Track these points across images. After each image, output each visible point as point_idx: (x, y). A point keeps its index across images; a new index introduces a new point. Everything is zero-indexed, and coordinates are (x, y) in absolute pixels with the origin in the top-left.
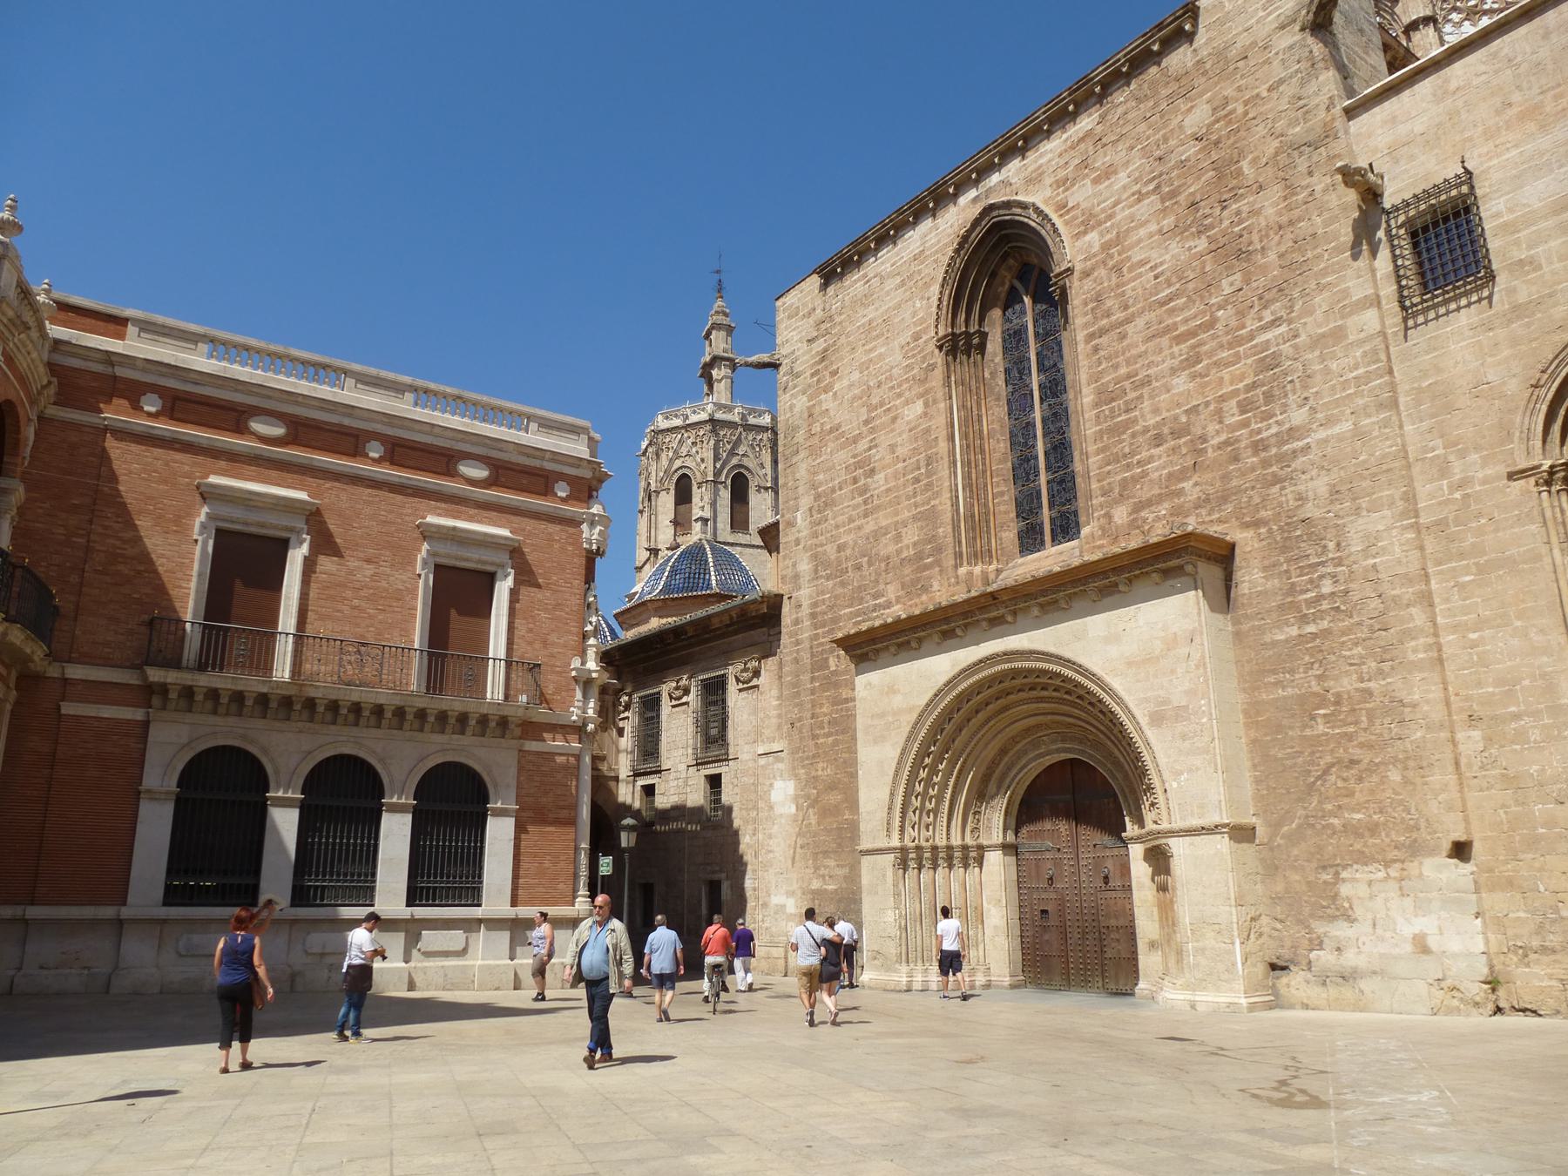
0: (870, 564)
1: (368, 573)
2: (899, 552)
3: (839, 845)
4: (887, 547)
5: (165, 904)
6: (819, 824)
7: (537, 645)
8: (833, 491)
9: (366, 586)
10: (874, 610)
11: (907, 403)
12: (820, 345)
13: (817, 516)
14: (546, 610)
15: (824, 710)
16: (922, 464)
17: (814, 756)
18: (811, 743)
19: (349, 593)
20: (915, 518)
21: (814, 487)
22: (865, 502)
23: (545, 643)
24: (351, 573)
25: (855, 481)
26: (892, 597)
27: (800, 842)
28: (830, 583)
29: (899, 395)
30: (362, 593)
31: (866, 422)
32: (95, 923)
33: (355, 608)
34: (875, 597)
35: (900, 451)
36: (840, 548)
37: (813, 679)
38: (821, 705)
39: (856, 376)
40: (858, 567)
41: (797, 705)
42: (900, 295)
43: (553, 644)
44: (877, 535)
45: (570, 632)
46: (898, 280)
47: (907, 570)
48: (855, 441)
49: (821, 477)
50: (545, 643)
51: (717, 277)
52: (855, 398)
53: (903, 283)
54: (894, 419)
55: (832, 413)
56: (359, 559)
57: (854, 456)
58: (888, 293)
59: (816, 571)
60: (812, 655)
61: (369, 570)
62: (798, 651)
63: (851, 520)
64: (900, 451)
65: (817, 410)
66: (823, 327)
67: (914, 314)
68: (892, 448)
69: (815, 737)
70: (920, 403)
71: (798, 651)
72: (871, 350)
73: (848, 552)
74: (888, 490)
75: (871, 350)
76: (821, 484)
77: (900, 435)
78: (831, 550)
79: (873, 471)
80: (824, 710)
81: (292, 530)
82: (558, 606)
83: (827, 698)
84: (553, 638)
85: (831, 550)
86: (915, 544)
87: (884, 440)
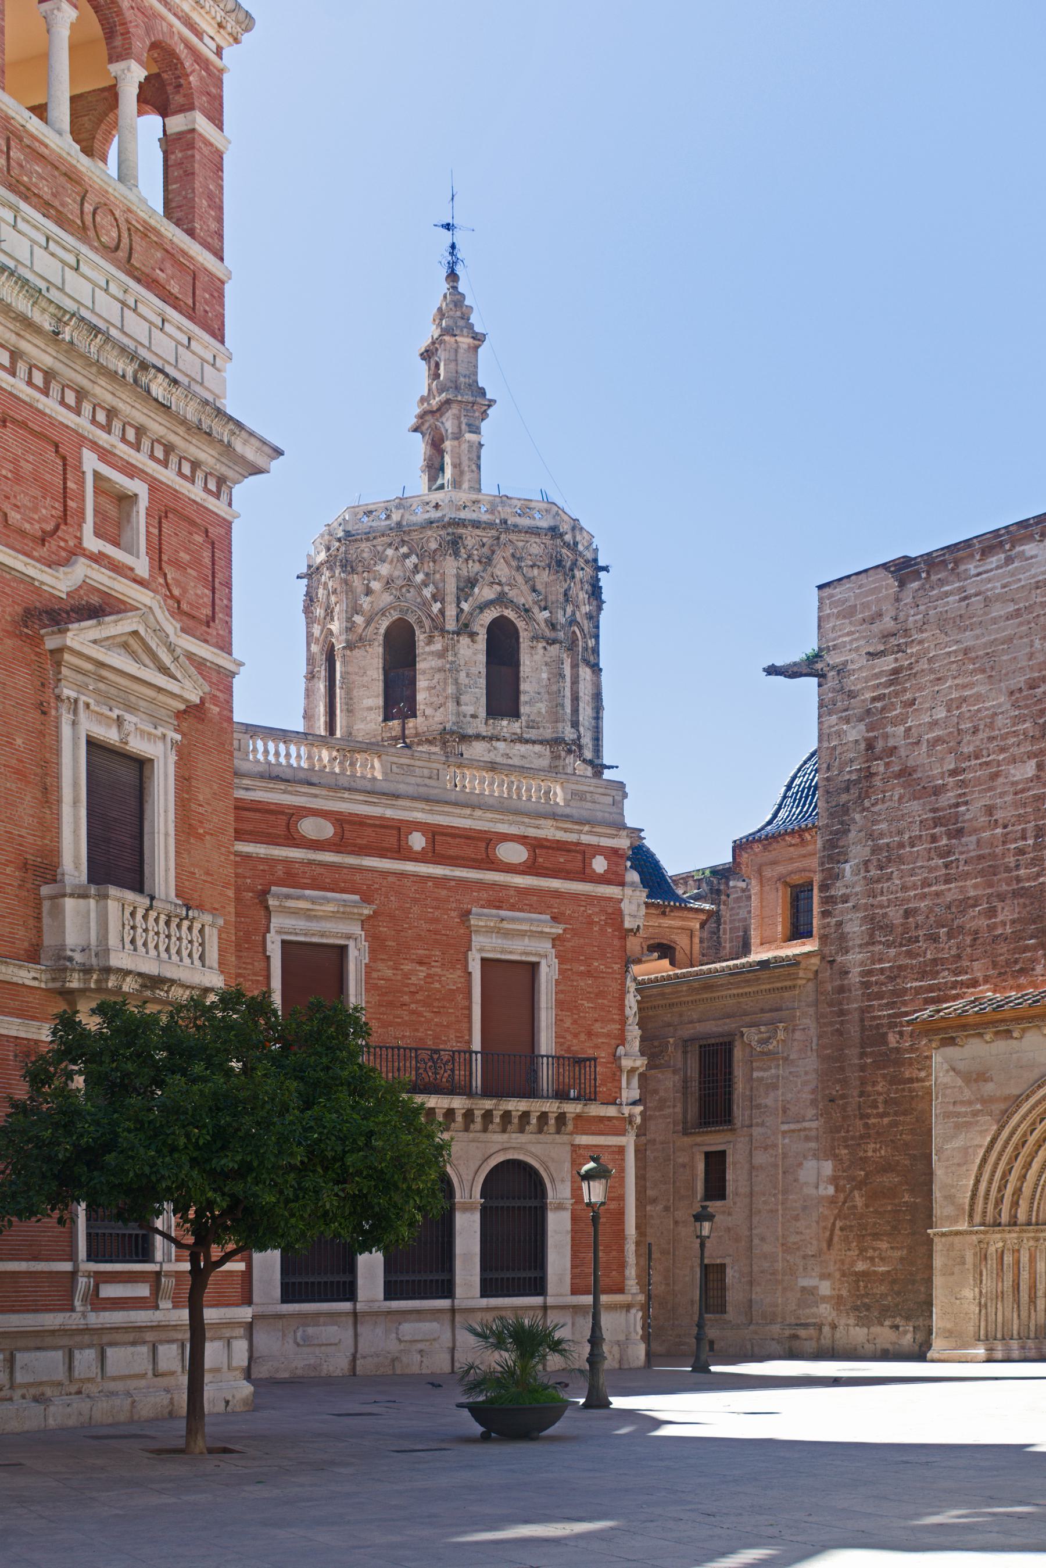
0: (950, 935)
1: (422, 975)
2: (991, 928)
3: (894, 1228)
4: (975, 920)
5: (483, 1295)
6: (867, 1206)
7: (583, 1037)
8: (901, 845)
9: (421, 988)
10: (953, 988)
11: (1014, 760)
12: (888, 663)
13: (874, 872)
14: (589, 999)
15: (879, 1088)
16: (1030, 833)
17: (862, 1137)
18: (859, 1123)
19: (406, 998)
20: (1015, 894)
21: (870, 836)
22: (947, 866)
23: (590, 1034)
24: (406, 976)
25: (934, 839)
26: (979, 975)
27: (839, 1224)
28: (892, 952)
29: (1003, 750)
30: (418, 997)
31: (954, 773)
32: (331, 1315)
33: (413, 1012)
34: (957, 972)
35: (999, 815)
36: (907, 914)
37: (863, 1055)
38: (874, 1084)
39: (941, 714)
40: (934, 938)
41: (839, 1081)
42: (1011, 628)
43: (598, 1035)
44: (966, 904)
45: (613, 1021)
46: (1012, 607)
47: (1003, 948)
48: (937, 791)
49: (883, 826)
50: (590, 1034)
51: (446, 237)
52: (938, 740)
53: (1017, 613)
54: (994, 776)
55: (903, 753)
56: (413, 961)
57: (934, 810)
58: (994, 621)
59: (872, 935)
60: (863, 1029)
61: (422, 972)
62: (842, 1023)
63: (926, 883)
64: (999, 815)
65: (880, 745)
66: (894, 641)
67: (1031, 656)
68: (990, 810)
69: (863, 1116)
70: (1033, 763)
71: (842, 1023)
72: (964, 687)
73: (920, 918)
74: (980, 857)
75: (964, 687)
76: (882, 835)
77: (1002, 795)
78: (895, 915)
79: (959, 833)
80: (879, 1088)
81: (349, 937)
82: (600, 994)
83: (884, 1076)
84: (597, 1027)
85: (895, 915)
86: (1013, 922)
87: (979, 802)
